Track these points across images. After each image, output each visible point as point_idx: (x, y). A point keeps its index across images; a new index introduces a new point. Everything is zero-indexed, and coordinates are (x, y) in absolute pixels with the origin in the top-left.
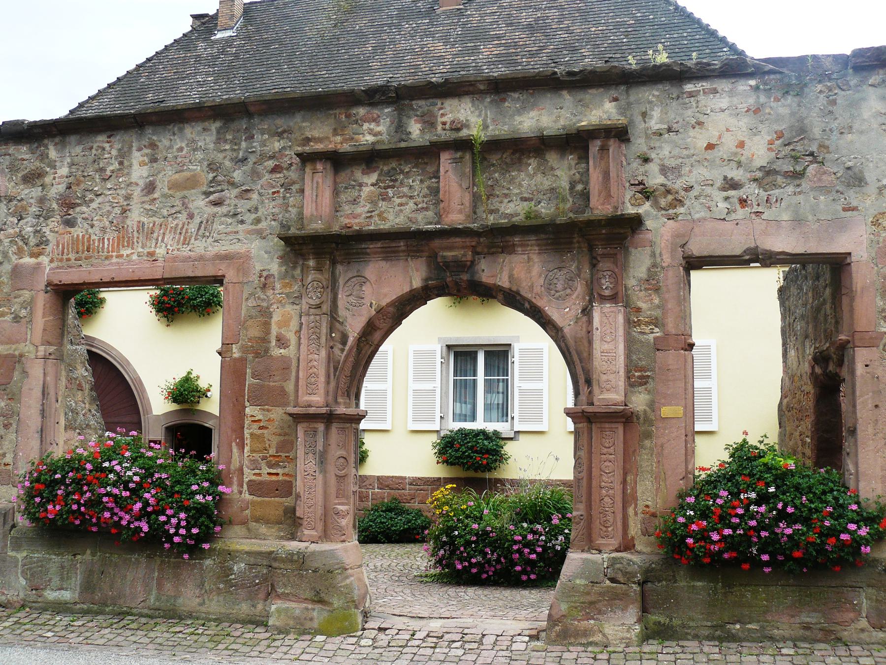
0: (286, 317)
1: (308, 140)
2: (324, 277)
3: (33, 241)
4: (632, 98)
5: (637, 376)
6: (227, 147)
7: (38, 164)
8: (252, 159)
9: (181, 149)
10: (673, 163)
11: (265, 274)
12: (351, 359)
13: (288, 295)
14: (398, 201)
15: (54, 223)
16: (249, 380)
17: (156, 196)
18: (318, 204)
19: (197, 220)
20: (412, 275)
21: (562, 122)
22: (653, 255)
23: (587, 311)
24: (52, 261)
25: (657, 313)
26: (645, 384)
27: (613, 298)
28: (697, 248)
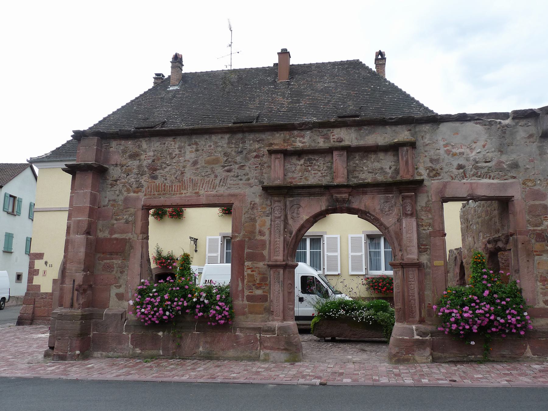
0: (264, 223)
1: (271, 144)
2: (281, 205)
3: (134, 186)
4: (417, 130)
5: (422, 248)
6: (233, 146)
8: (245, 152)
10: (435, 157)
11: (253, 203)
12: (294, 241)
13: (264, 212)
14: (313, 172)
15: (145, 178)
16: (246, 251)
17: (198, 167)
18: (277, 173)
19: (219, 178)
20: (322, 204)
21: (386, 140)
22: (428, 196)
23: (399, 220)
24: (145, 195)
25: (431, 221)
26: (426, 251)
27: (412, 215)
28: (448, 194)
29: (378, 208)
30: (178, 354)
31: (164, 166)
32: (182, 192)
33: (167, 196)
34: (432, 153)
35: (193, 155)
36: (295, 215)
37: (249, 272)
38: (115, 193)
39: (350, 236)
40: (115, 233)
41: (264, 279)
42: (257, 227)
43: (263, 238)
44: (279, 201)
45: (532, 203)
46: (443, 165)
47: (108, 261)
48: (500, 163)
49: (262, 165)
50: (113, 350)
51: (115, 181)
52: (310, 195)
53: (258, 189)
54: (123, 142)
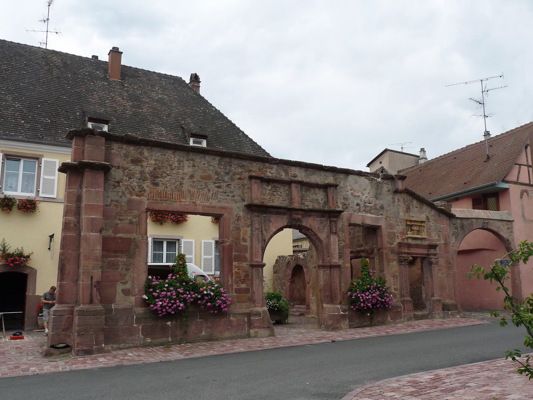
3: (137, 189)
4: (337, 177)
7: (139, 156)
8: (231, 174)
9: (204, 164)
10: (346, 197)
14: (277, 196)
16: (234, 253)
17: (195, 180)
19: (211, 192)
20: (284, 221)
24: (148, 199)
27: (336, 233)
29: (317, 227)
30: (183, 339)
31: (165, 175)
32: (181, 200)
33: (169, 202)
34: (344, 193)
35: (191, 170)
36: (267, 227)
37: (236, 270)
38: (118, 194)
39: (203, 241)
40: (119, 232)
41: (247, 276)
42: (241, 234)
43: (245, 244)
44: (258, 216)
45: (389, 231)
46: (350, 202)
47: (113, 259)
48: (376, 205)
49: (243, 186)
50: (124, 342)
51: (117, 182)
52: (277, 213)
53: (242, 205)
54: (125, 146)
